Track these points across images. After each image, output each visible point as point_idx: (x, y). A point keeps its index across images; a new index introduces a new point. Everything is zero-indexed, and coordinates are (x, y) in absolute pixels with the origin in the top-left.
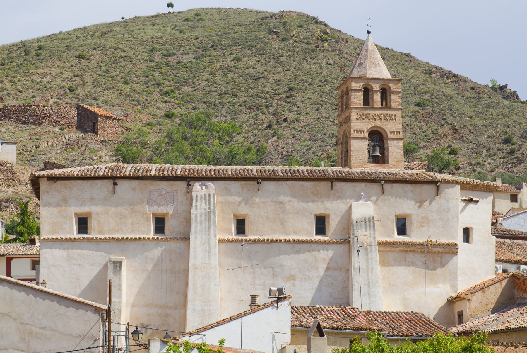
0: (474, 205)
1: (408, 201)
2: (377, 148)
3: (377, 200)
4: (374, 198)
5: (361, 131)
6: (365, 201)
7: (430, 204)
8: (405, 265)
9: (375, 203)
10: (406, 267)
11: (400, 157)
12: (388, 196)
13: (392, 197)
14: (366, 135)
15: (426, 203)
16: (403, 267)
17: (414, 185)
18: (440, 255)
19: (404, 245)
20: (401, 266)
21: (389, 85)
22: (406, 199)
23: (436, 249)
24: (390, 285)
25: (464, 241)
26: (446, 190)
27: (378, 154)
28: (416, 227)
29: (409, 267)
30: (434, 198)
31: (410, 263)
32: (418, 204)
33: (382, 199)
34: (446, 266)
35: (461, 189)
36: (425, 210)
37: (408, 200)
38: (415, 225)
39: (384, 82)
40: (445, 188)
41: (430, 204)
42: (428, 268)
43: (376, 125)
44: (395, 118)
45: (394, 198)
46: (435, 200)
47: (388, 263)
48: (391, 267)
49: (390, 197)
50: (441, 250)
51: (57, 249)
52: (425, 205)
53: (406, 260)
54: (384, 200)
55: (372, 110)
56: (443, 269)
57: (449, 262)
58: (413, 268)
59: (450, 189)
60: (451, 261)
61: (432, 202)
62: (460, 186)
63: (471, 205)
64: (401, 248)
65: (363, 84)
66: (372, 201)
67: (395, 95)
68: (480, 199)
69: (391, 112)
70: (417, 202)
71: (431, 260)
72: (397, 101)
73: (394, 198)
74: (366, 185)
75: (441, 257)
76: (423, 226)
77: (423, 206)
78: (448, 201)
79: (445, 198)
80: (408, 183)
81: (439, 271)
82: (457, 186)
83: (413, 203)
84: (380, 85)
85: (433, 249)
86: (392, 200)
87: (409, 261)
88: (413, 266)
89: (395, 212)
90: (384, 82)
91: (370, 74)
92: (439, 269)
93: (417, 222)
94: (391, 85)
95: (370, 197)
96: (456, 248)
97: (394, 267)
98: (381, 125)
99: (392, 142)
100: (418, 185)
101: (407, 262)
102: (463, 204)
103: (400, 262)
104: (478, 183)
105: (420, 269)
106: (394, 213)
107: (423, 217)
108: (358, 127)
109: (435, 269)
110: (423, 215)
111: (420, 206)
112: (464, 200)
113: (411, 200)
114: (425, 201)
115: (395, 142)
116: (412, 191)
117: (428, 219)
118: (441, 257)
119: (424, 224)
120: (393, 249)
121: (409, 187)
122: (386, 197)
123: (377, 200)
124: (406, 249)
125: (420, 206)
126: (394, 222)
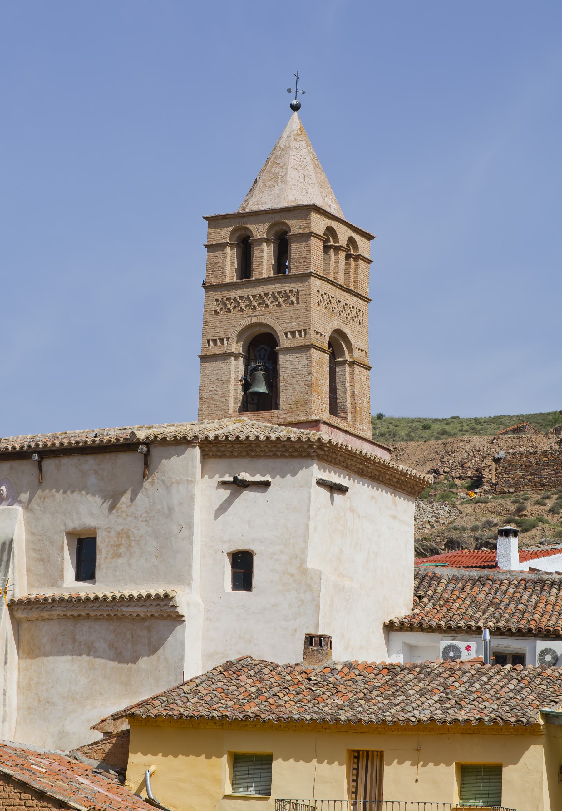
0: (258, 494)
1: (89, 497)
2: (260, 374)
3: (30, 500)
4: (24, 497)
5: (321, 335)
6: (9, 505)
7: (132, 500)
8: (72, 653)
9: (27, 507)
10: (75, 657)
11: (303, 390)
12: (51, 490)
13: (58, 491)
14: (237, 347)
15: (126, 498)
16: (69, 657)
17: (100, 456)
18: (147, 623)
19: (63, 604)
20: (64, 654)
21: (287, 221)
22: (83, 492)
23: (130, 609)
24: (39, 701)
25: (235, 587)
26: (164, 461)
27: (262, 388)
28: (106, 558)
29: (79, 658)
30: (141, 486)
31: (82, 647)
32: (107, 505)
33: (40, 497)
34: (160, 651)
35: (205, 456)
36: (124, 515)
37: (87, 494)
38: (104, 555)
39: (277, 218)
40: (162, 458)
41: (132, 500)
42: (120, 658)
43: (255, 320)
44: (298, 299)
45: (61, 491)
46: (143, 490)
47: (39, 648)
48: (45, 660)
49: (54, 490)
50: (142, 611)
51: (292, 760)
52: (123, 503)
53: (74, 641)
54: (44, 498)
55: (248, 288)
56: (154, 657)
57: (166, 639)
58: (88, 658)
59: (174, 459)
60: (170, 639)
61: (137, 495)
62: (197, 450)
63: (248, 495)
64: (58, 611)
65: (231, 228)
66: (21, 502)
67: (299, 245)
68: (273, 477)
69: (288, 287)
70: (105, 498)
71: (129, 636)
72: (304, 258)
73: (61, 491)
74: (11, 468)
75: (149, 629)
76: (119, 555)
77: (119, 505)
78: (168, 488)
79: (163, 482)
80: (87, 454)
81: (143, 662)
82: (189, 450)
83: (98, 499)
84: (267, 225)
85: (124, 609)
86: (59, 496)
87: (80, 643)
88: (89, 655)
89: (65, 525)
90: (277, 218)
91: (254, 204)
92: (145, 658)
93: (107, 546)
94: (290, 223)
95: (19, 494)
96: (171, 604)
97: (51, 658)
98: (266, 320)
99: (288, 357)
100: (108, 456)
101: (77, 644)
102: (225, 493)
103: (62, 645)
104: (304, 439)
105: (103, 661)
106: (63, 528)
107: (118, 534)
108: (217, 330)
109: (135, 660)
110: (119, 529)
111: (112, 508)
112: (224, 484)
113: (94, 495)
114: (123, 493)
115: (294, 356)
116: (96, 472)
117: (128, 537)
118: (149, 629)
119: (122, 550)
120: (45, 615)
121: (90, 462)
122: (47, 491)
123: (30, 500)
124: (69, 613)
125: (112, 508)
126: (62, 549)
